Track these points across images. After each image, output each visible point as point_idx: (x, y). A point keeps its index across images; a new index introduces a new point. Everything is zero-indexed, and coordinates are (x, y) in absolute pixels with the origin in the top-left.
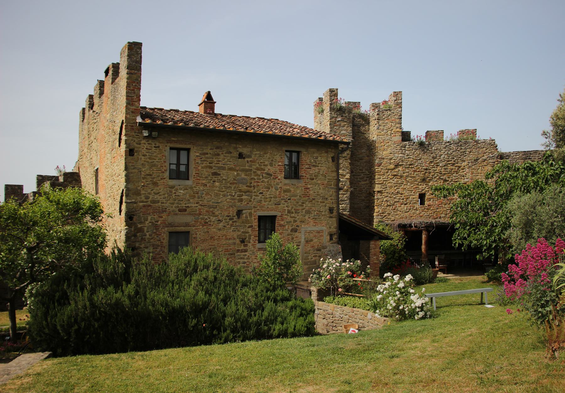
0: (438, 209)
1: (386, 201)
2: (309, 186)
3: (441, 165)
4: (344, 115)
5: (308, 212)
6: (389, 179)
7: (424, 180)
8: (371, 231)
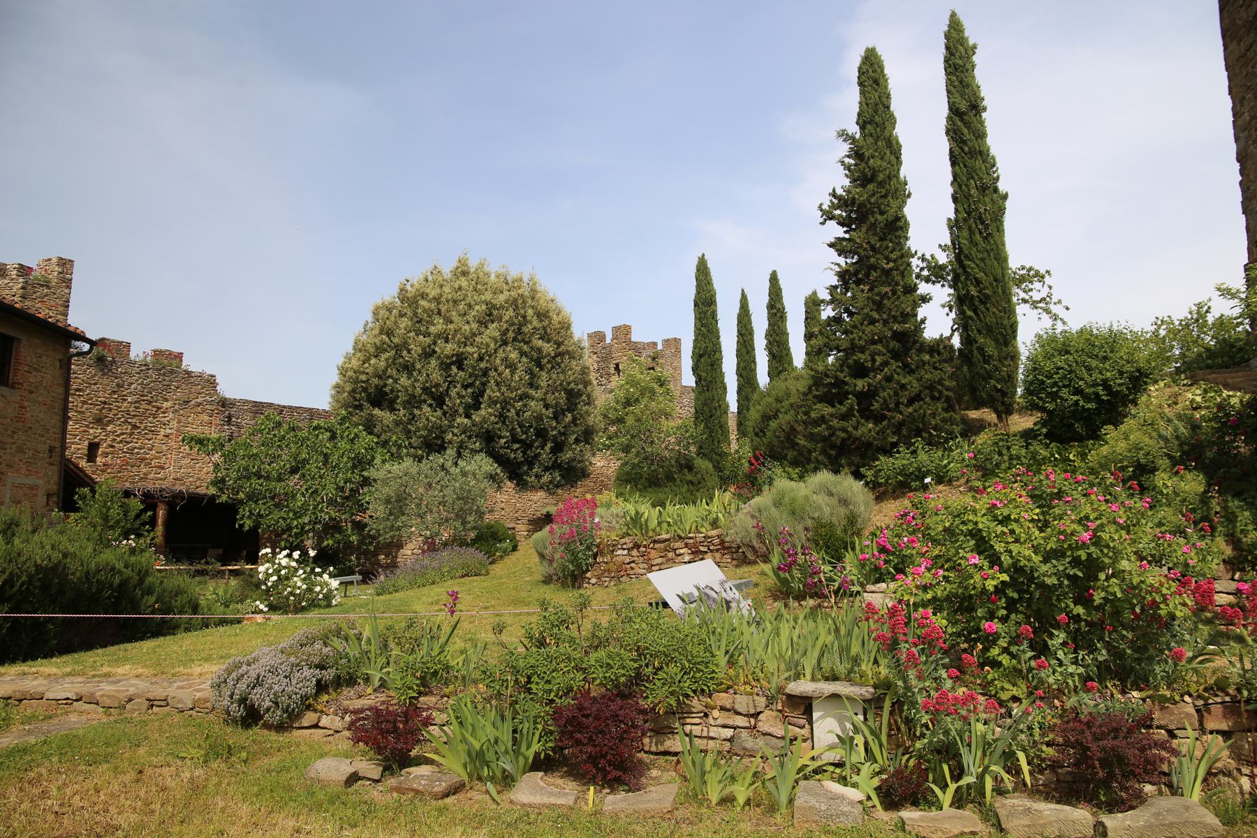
0: (120, 472)
2: (26, 404)
3: (129, 399)
5: (20, 450)
7: (99, 421)
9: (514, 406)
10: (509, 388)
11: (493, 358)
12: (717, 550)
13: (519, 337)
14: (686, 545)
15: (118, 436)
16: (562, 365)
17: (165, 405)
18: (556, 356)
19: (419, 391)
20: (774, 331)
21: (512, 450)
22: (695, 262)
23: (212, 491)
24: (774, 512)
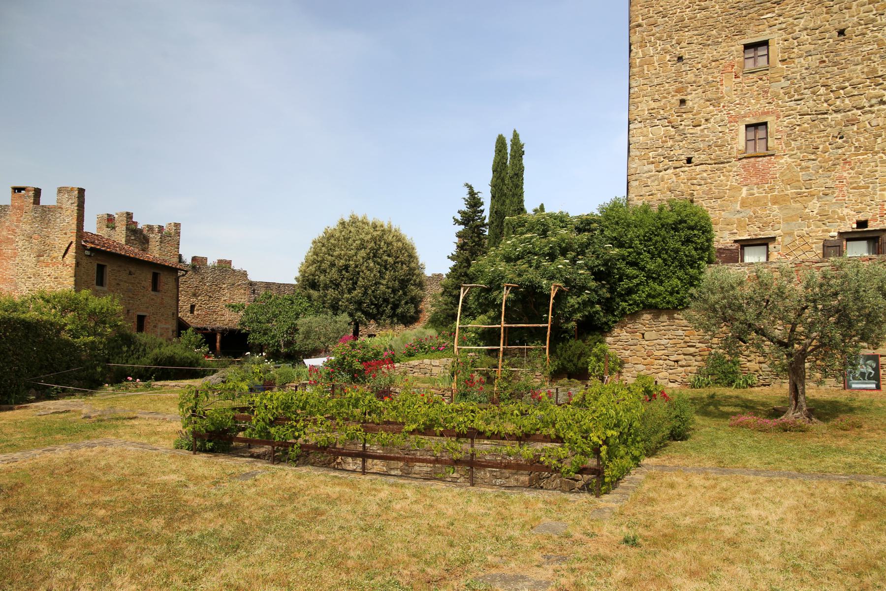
5: (162, 315)
7: (195, 295)
10: (369, 281)
17: (224, 286)
19: (328, 282)
23: (239, 327)
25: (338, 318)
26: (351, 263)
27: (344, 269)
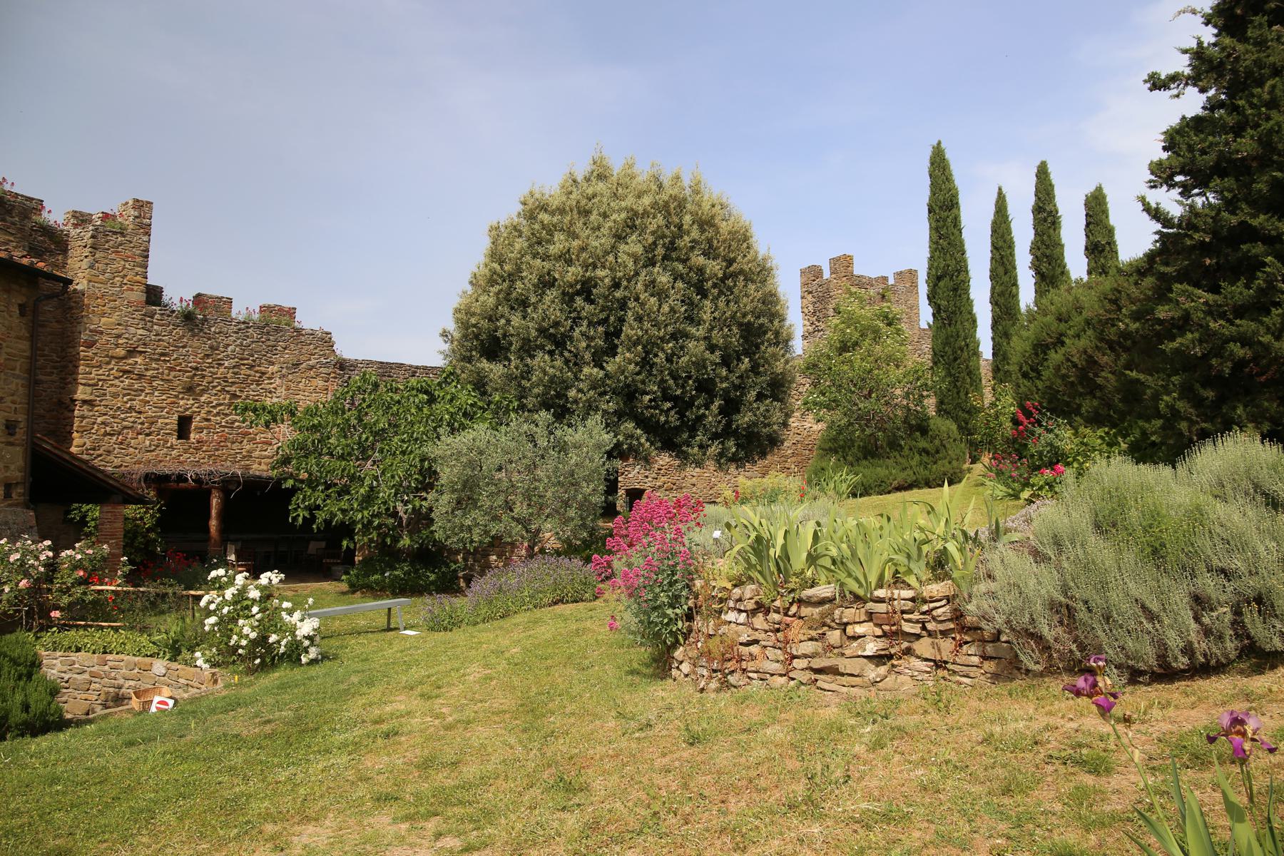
0: (217, 450)
1: (103, 423)
3: (226, 364)
4: (8, 218)
6: (112, 377)
7: (190, 390)
8: (105, 482)
9: (663, 349)
10: (656, 325)
11: (633, 282)
12: (945, 633)
13: (674, 255)
14: (870, 616)
15: (214, 407)
16: (736, 291)
18: (725, 277)
19: (534, 333)
20: (1043, 242)
21: (662, 411)
22: (928, 153)
24: (1101, 551)
25: (571, 435)
26: (600, 273)
27: (578, 293)
